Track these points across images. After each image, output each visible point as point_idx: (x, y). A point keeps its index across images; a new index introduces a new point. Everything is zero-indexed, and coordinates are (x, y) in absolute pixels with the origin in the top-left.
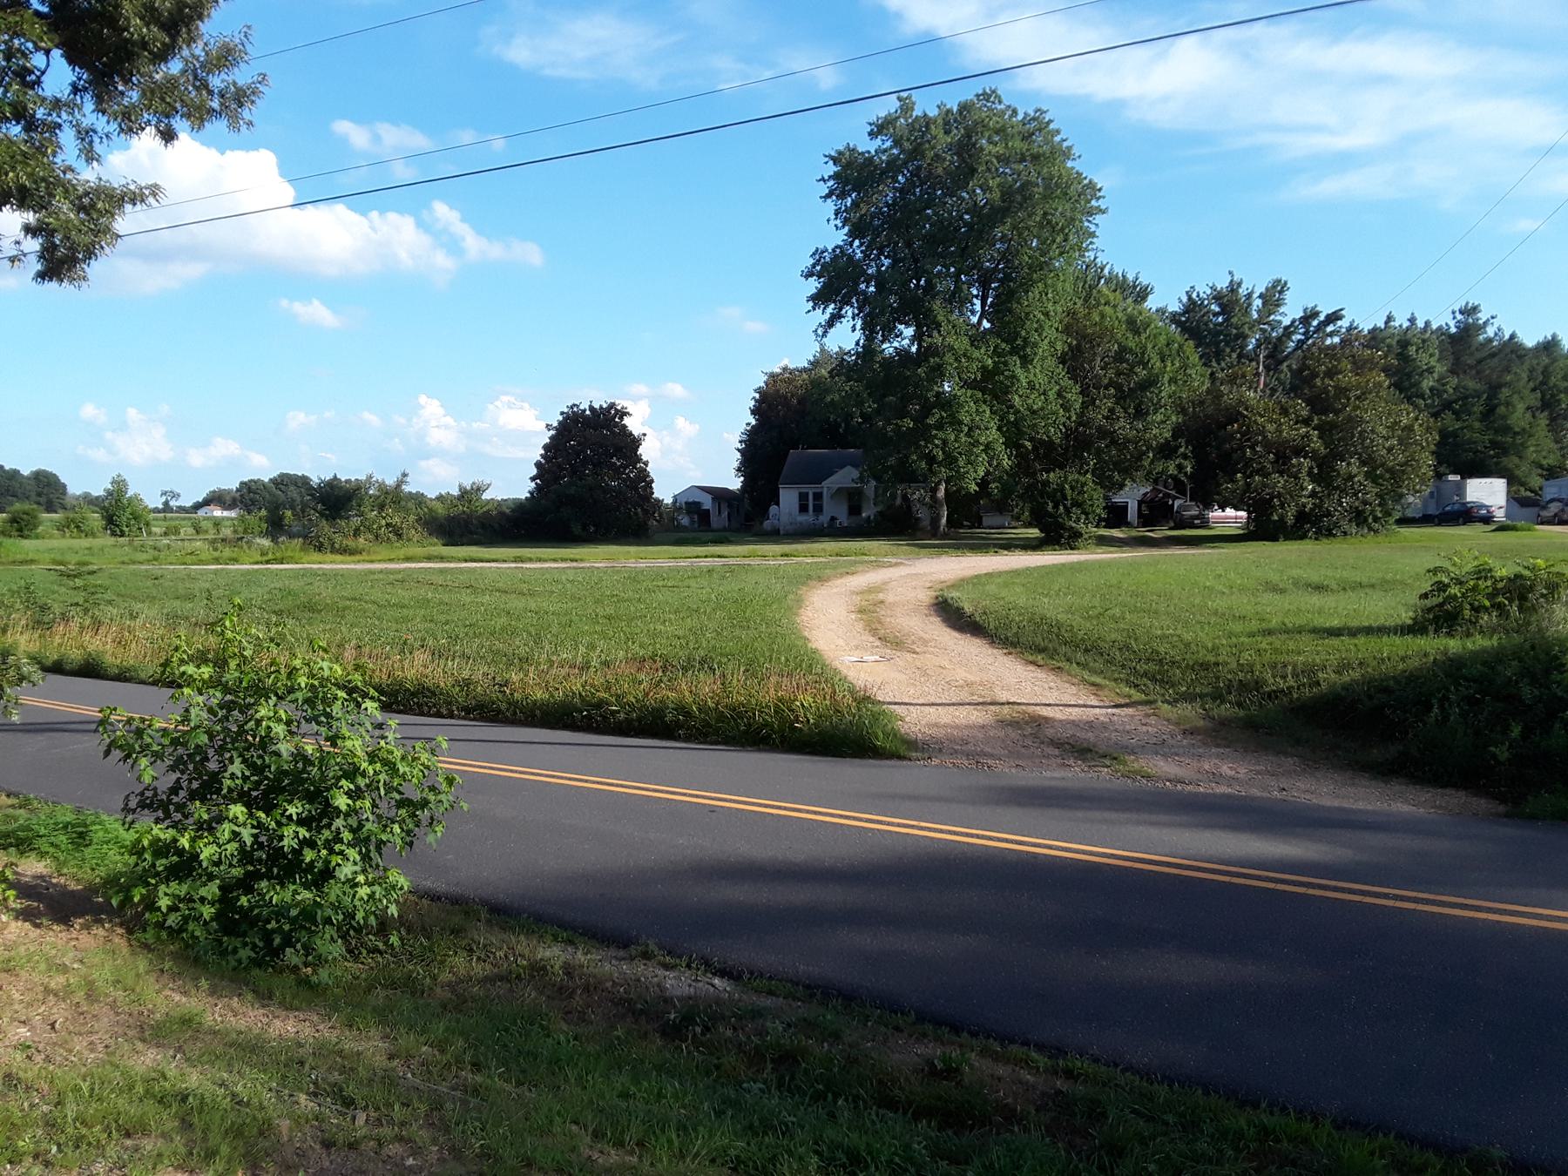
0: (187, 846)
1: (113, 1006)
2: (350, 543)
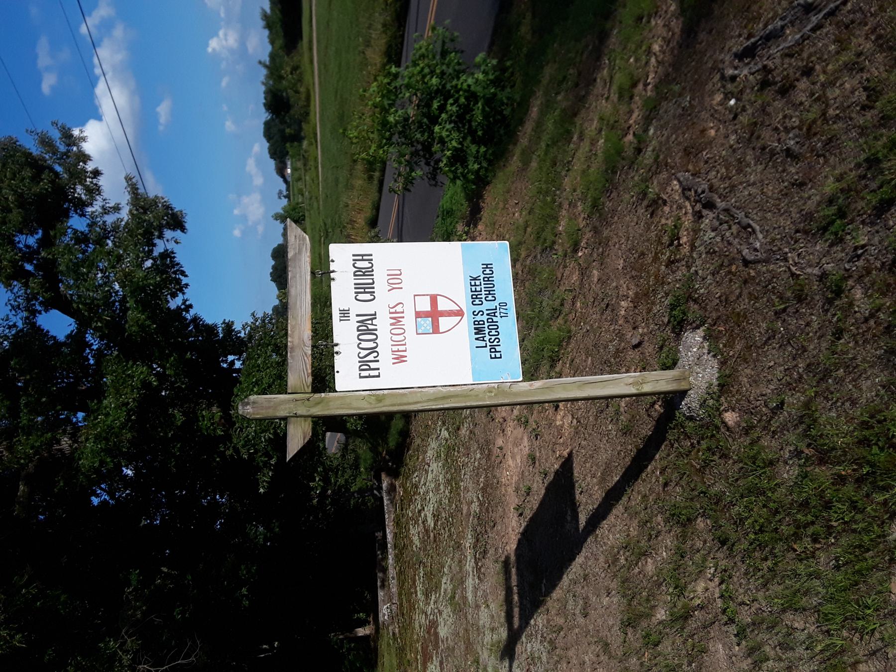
0: (450, 152)
1: (513, 183)
2: (303, 96)
